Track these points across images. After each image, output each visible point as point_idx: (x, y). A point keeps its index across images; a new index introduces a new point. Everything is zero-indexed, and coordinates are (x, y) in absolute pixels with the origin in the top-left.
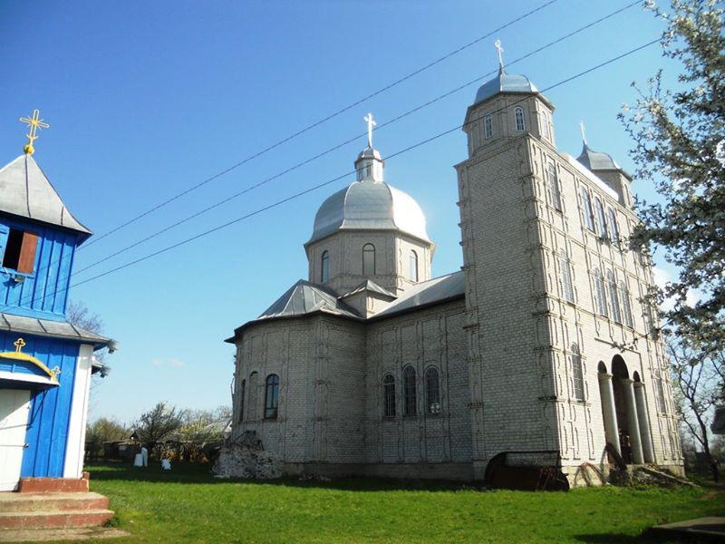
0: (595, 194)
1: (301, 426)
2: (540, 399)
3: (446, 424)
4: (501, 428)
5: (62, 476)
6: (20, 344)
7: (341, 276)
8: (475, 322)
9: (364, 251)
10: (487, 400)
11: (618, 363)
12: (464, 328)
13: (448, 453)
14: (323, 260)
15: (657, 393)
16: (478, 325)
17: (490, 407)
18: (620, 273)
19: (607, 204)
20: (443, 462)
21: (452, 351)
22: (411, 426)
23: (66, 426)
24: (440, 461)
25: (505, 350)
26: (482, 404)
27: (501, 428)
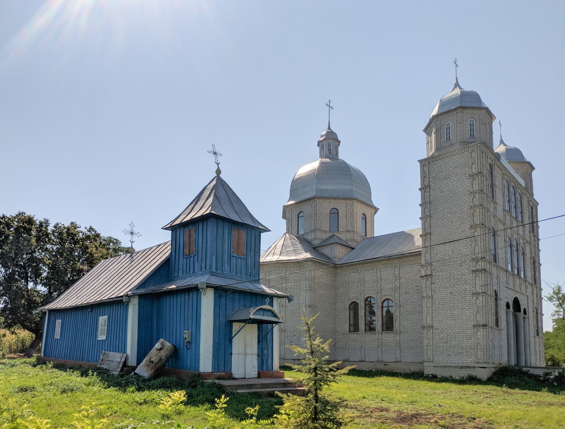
0: (519, 191)
1: (295, 336)
2: (474, 326)
3: (398, 338)
4: (445, 343)
5: (272, 370)
6: (267, 301)
7: (314, 231)
8: (430, 273)
9: (330, 213)
10: (436, 325)
11: (516, 302)
12: (421, 277)
13: (398, 356)
14: (298, 217)
15: (535, 323)
16: (431, 275)
17: (438, 329)
18: (521, 241)
19: (518, 190)
20: (395, 362)
21: (403, 290)
22: (370, 337)
23: (271, 341)
24: (393, 361)
25: (451, 293)
26: (432, 327)
27: (445, 343)
